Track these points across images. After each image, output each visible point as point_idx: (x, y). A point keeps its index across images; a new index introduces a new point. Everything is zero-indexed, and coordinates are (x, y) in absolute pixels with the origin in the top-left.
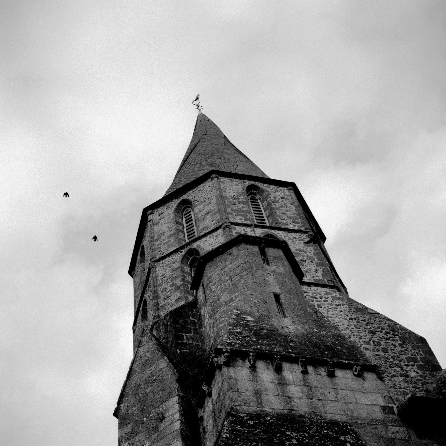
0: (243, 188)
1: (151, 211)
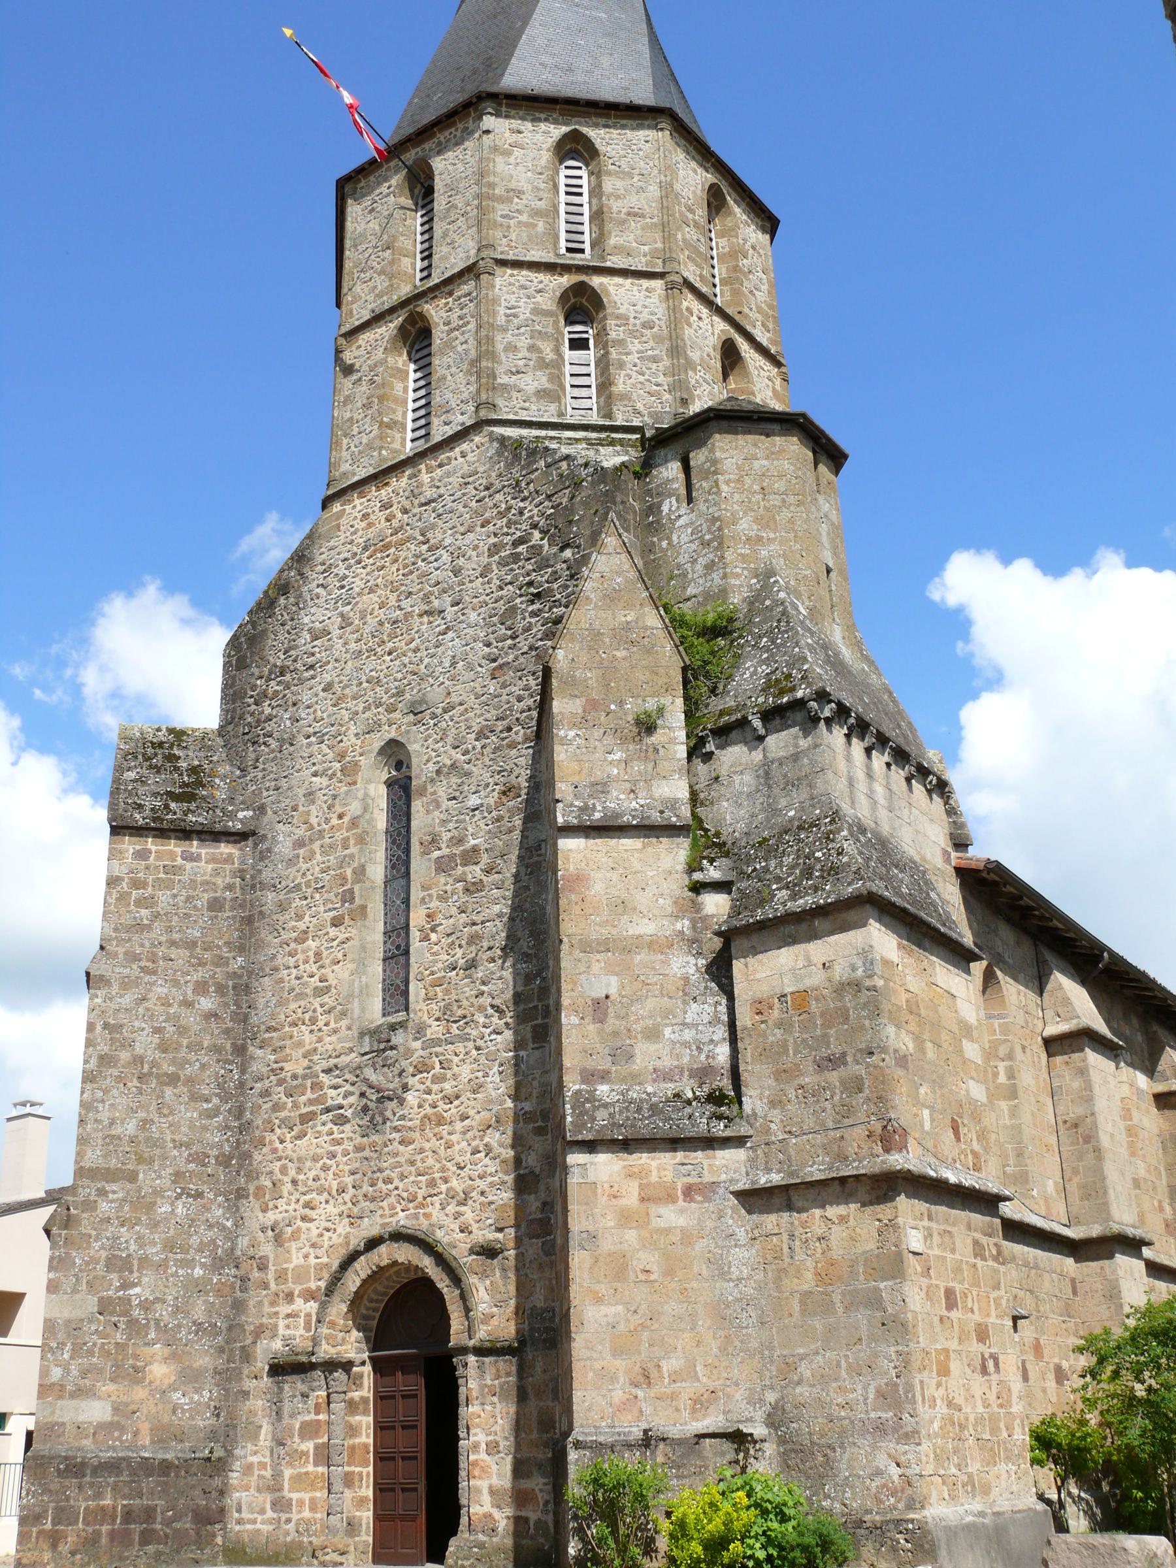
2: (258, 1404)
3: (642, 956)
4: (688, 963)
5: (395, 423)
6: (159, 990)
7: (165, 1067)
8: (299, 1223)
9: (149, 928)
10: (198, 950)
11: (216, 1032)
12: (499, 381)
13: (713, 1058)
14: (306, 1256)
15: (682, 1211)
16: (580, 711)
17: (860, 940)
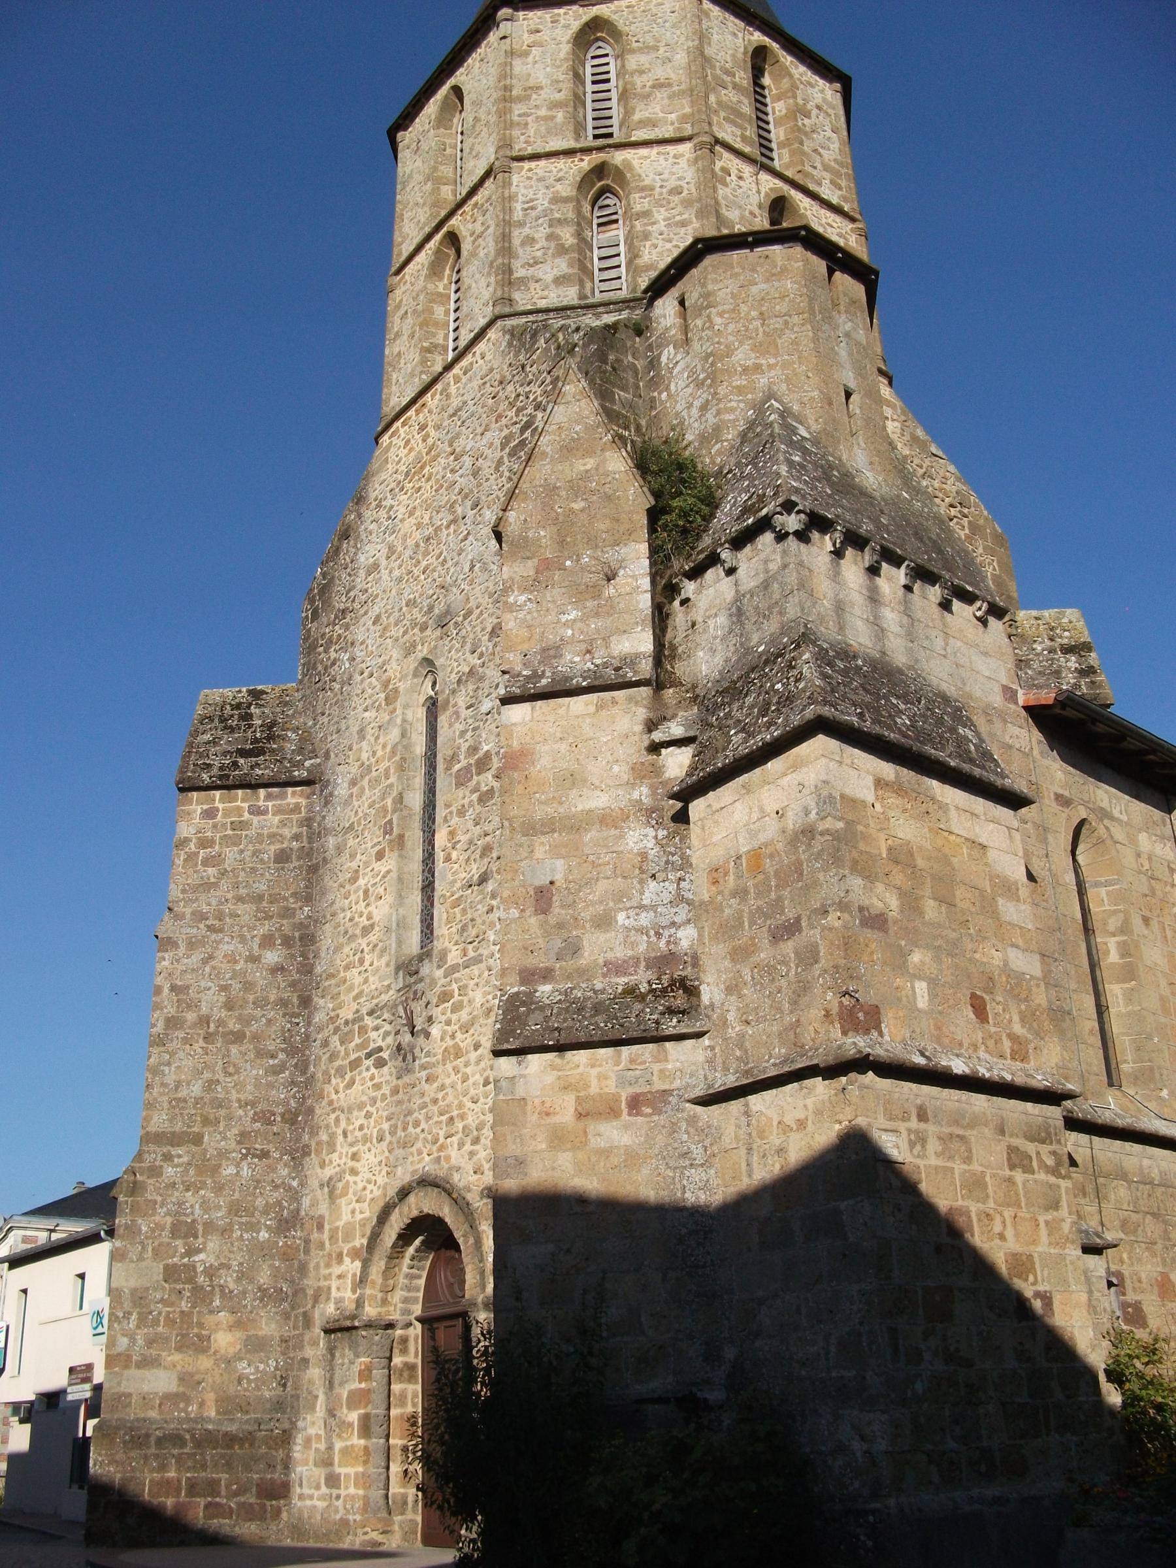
0: (745, 48)
1: (510, 11)
2: (315, 1373)
3: (593, 833)
4: (646, 836)
5: (436, 346)
6: (226, 947)
7: (231, 1026)
8: (348, 1177)
9: (215, 885)
10: (265, 904)
11: (283, 985)
12: (516, 275)
13: (675, 943)
14: (353, 1212)
15: (626, 1127)
16: (532, 573)
17: (812, 776)
